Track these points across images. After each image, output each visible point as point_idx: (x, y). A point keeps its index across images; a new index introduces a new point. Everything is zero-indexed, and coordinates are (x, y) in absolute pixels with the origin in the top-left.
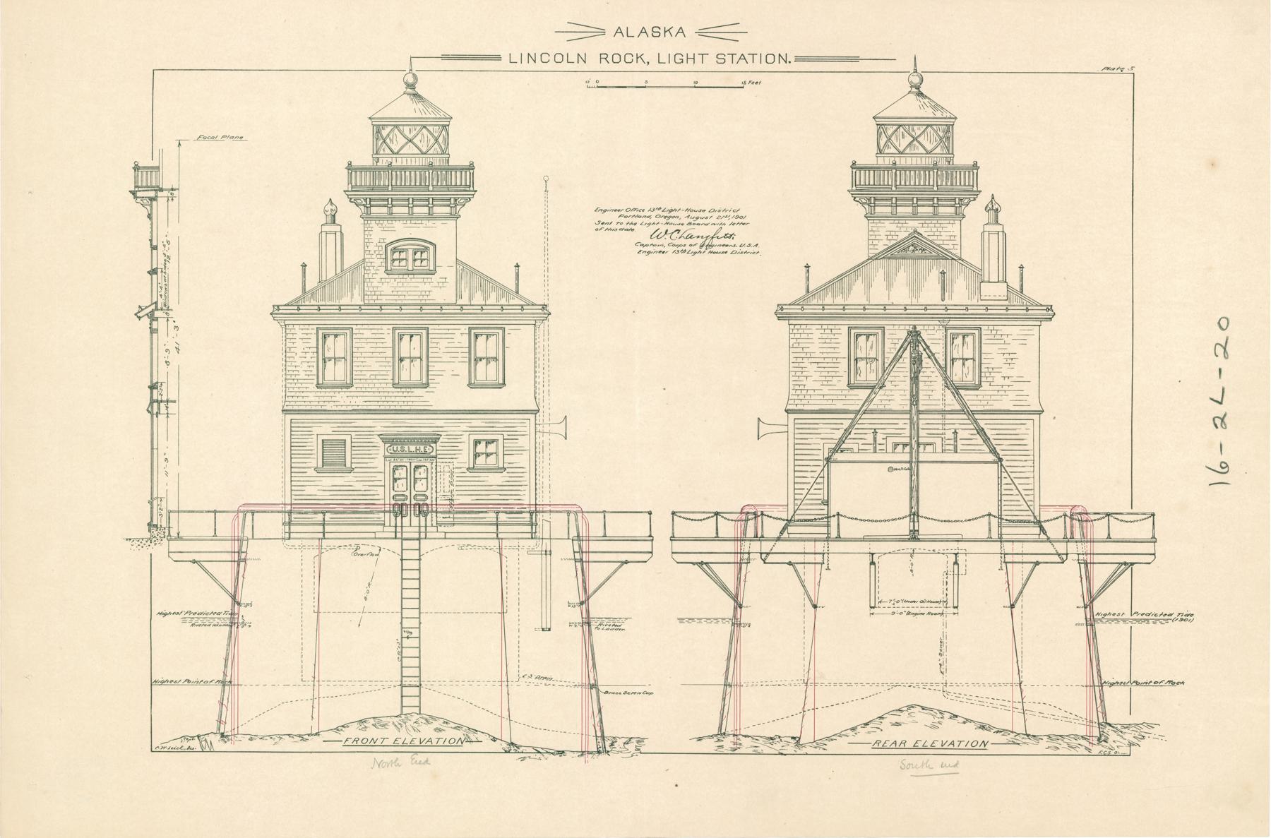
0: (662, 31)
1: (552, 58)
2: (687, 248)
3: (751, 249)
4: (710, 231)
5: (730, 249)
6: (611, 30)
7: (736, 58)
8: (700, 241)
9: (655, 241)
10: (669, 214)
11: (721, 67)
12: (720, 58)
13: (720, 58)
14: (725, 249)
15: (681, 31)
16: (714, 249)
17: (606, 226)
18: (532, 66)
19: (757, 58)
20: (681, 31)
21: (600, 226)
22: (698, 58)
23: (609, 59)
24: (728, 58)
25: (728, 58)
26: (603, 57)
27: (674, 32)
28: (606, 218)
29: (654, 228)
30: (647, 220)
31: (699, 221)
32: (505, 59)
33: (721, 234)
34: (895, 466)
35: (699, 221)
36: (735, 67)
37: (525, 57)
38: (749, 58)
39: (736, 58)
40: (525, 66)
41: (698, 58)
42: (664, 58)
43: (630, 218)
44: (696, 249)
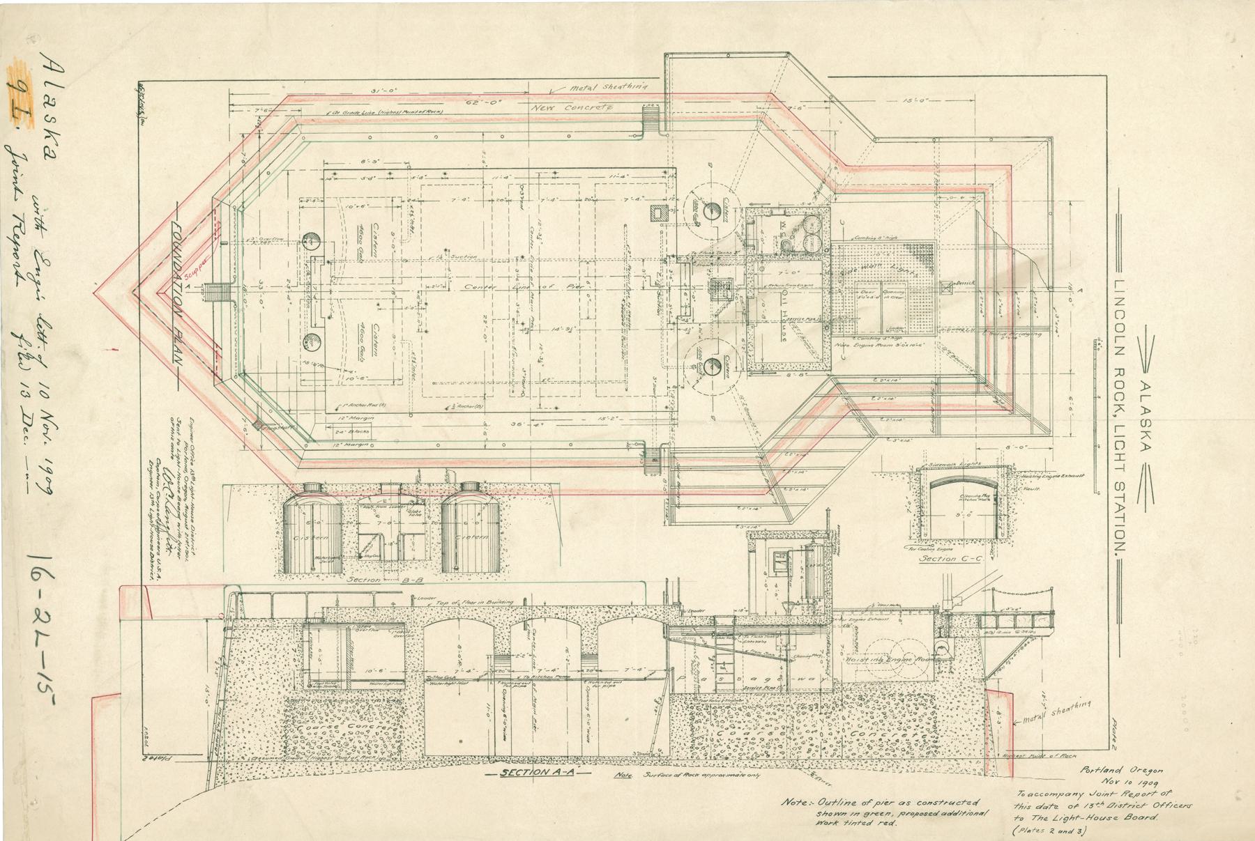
0: (1146, 429)
1: (1119, 321)
4: (173, 531)
6: (1147, 378)
7: (1120, 501)
8: (164, 520)
14: (155, 548)
15: (1147, 447)
19: (1120, 521)
20: (1147, 447)
22: (1120, 464)
23: (1119, 378)
24: (1120, 493)
25: (1120, 493)
27: (1146, 440)
33: (171, 542)
37: (1120, 295)
38: (1120, 514)
39: (1120, 501)
42: (1120, 431)
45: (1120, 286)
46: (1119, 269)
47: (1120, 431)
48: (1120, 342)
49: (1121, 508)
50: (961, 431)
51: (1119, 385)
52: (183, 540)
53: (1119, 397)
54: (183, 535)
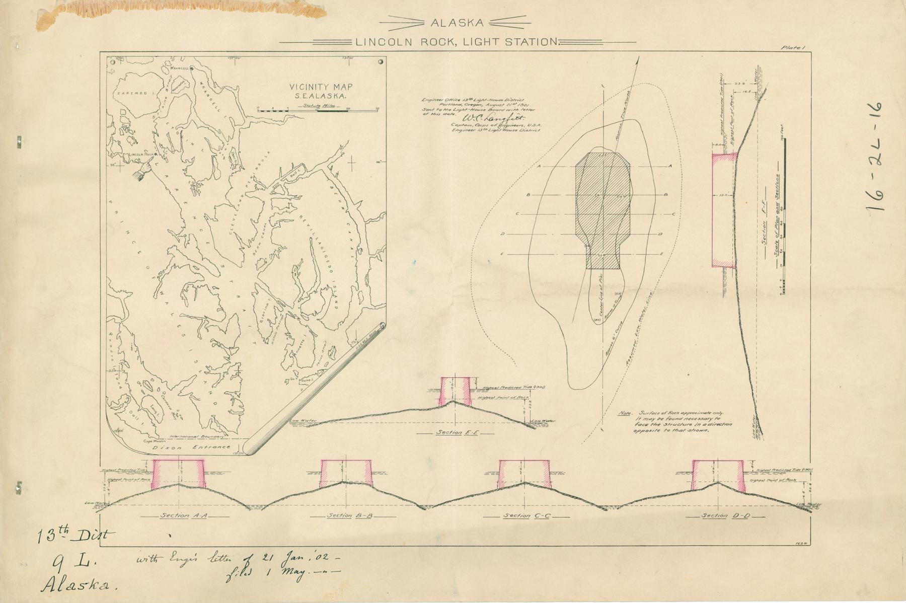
0: (466, 22)
1: (387, 42)
2: (488, 128)
3: (535, 128)
4: (506, 115)
5: (519, 128)
6: (428, 22)
7: (520, 41)
8: (499, 122)
9: (466, 122)
10: (474, 103)
11: (509, 48)
12: (509, 41)
13: (509, 41)
14: (515, 128)
15: (480, 22)
16: (508, 128)
17: (431, 112)
18: (372, 48)
19: (535, 41)
20: (480, 22)
21: (426, 112)
22: (493, 42)
23: (428, 42)
24: (514, 42)
25: (514, 42)
26: (424, 41)
27: (475, 23)
28: (430, 106)
29: (465, 113)
30: (460, 108)
31: (496, 108)
32: (354, 42)
33: (514, 117)
34: (796, 50)
35: (496, 108)
36: (519, 48)
37: (367, 41)
38: (529, 42)
39: (520, 41)
40: (367, 48)
41: (493, 42)
42: (468, 42)
43: (448, 107)
44: (496, 128)
45: (361, 42)
46: (348, 42)
47: (468, 42)
48: (402, 42)
49: (525, 41)
50: (451, 510)
51: (433, 42)
52: (512, 107)
53: (442, 42)
54: (509, 108)
